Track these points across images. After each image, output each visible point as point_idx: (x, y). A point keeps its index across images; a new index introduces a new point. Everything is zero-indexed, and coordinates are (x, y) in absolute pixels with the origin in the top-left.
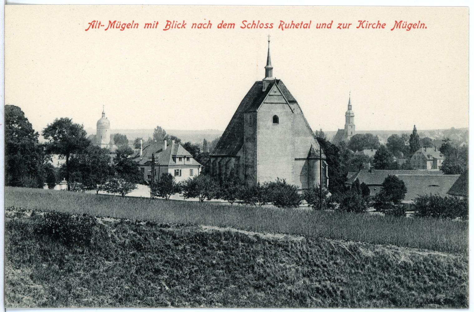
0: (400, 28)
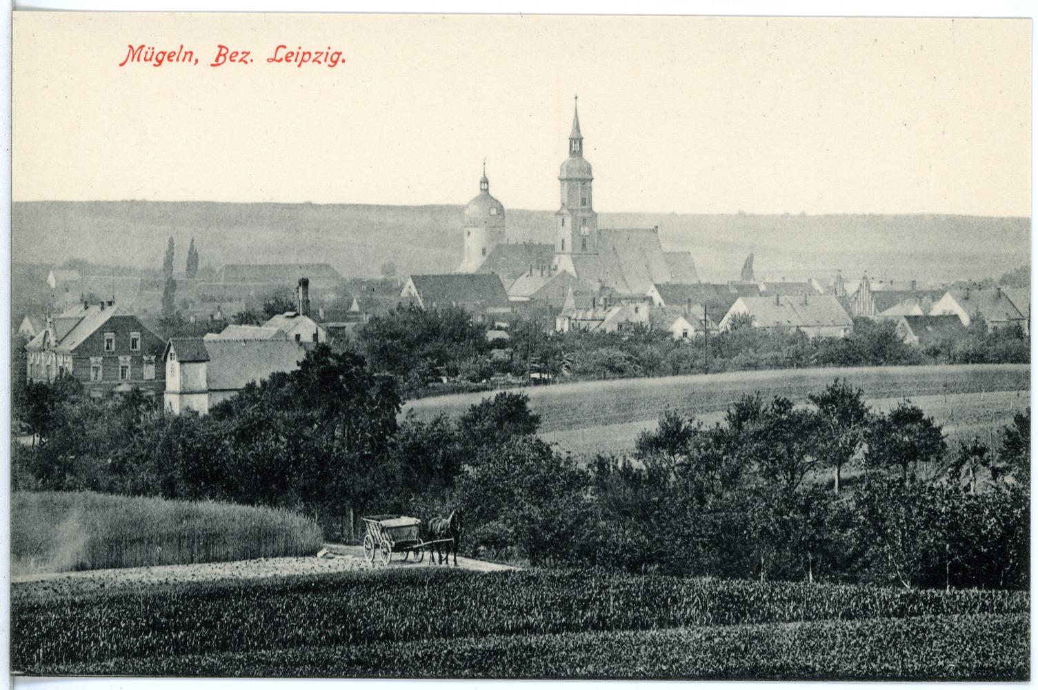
0: (138, 60)
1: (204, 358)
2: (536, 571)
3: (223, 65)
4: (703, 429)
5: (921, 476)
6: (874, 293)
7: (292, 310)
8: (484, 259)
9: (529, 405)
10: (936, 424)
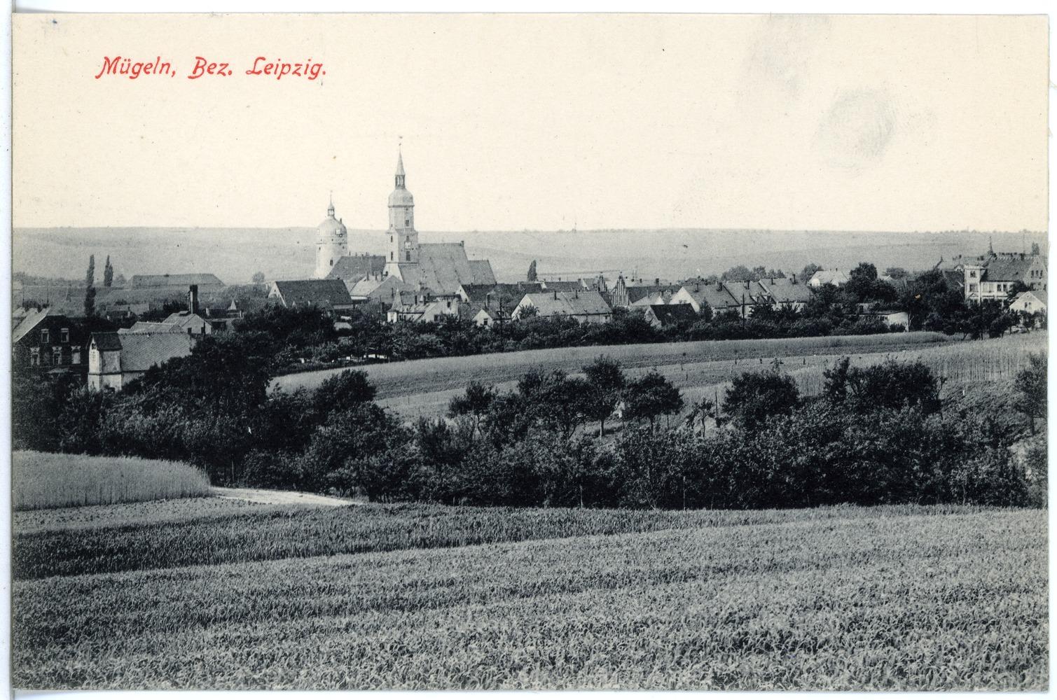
1: (117, 347)
2: (375, 505)
3: (200, 78)
4: (499, 394)
5: (664, 425)
6: (628, 288)
7: (186, 309)
8: (332, 267)
9: (368, 378)
10: (675, 385)
